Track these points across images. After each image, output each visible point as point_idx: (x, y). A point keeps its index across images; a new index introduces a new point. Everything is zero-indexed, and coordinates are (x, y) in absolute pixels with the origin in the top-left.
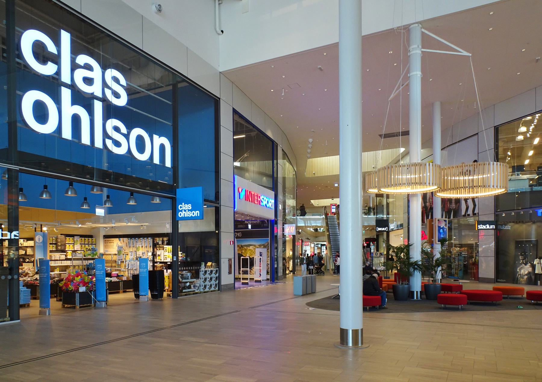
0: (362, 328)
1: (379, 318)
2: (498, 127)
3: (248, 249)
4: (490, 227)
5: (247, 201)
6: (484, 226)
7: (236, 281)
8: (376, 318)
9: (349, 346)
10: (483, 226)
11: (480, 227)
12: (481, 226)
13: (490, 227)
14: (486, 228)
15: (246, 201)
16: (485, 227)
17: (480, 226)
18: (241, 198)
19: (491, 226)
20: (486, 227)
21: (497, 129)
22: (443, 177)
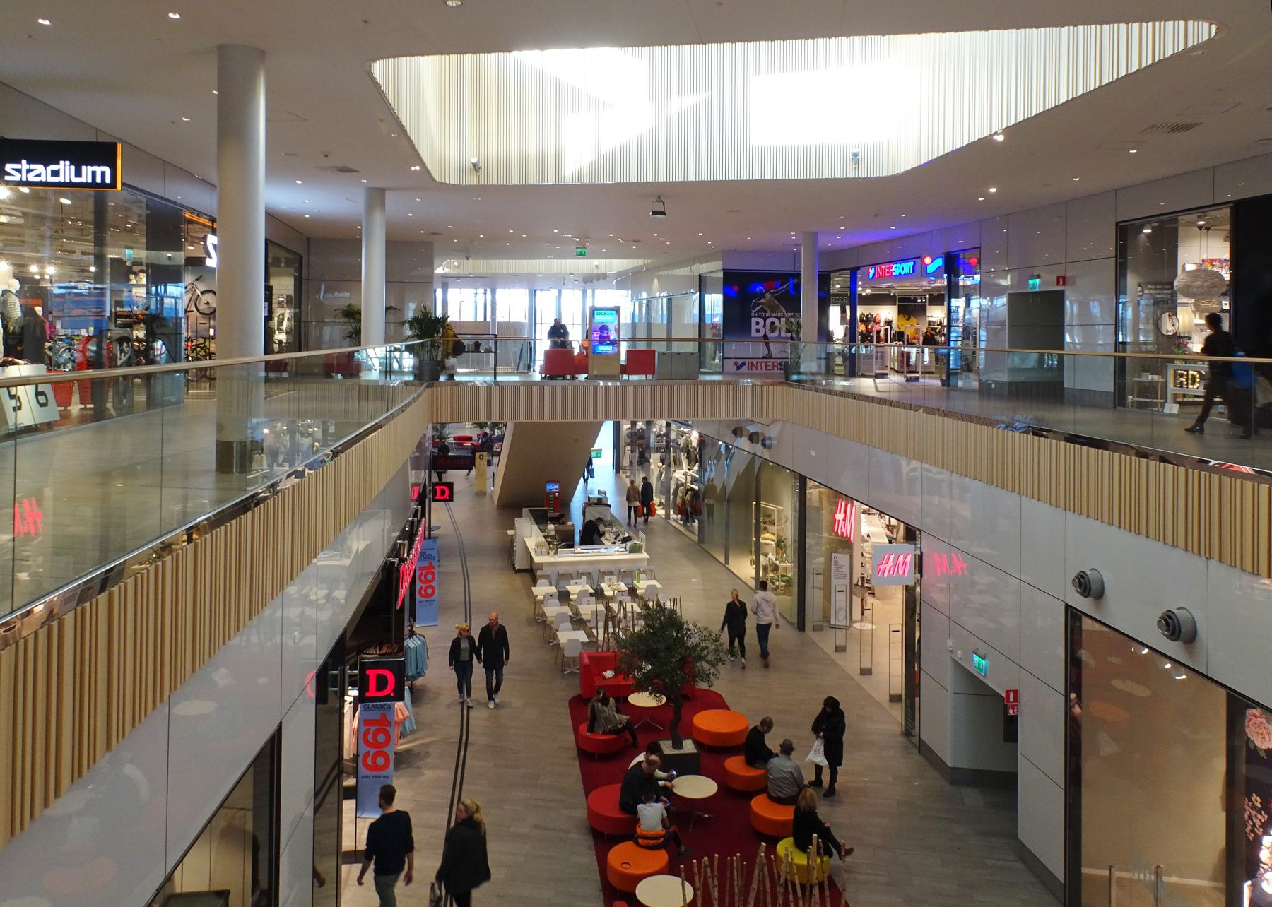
0: (46, 810)
1: (1207, 651)
2: (12, 205)
3: (331, 296)
4: (78, 174)
5: (1165, 543)
6: (39, 168)
7: (275, 275)
8: (727, 526)
9: (390, 511)
10: (32, 166)
11: (19, 171)
12: (24, 165)
13: (78, 174)
14: (55, 179)
15: (1061, 510)
16: (49, 173)
17: (17, 166)
18: (1194, 551)
19: (84, 168)
20: (55, 173)
21: (890, 625)
22: (756, 519)
